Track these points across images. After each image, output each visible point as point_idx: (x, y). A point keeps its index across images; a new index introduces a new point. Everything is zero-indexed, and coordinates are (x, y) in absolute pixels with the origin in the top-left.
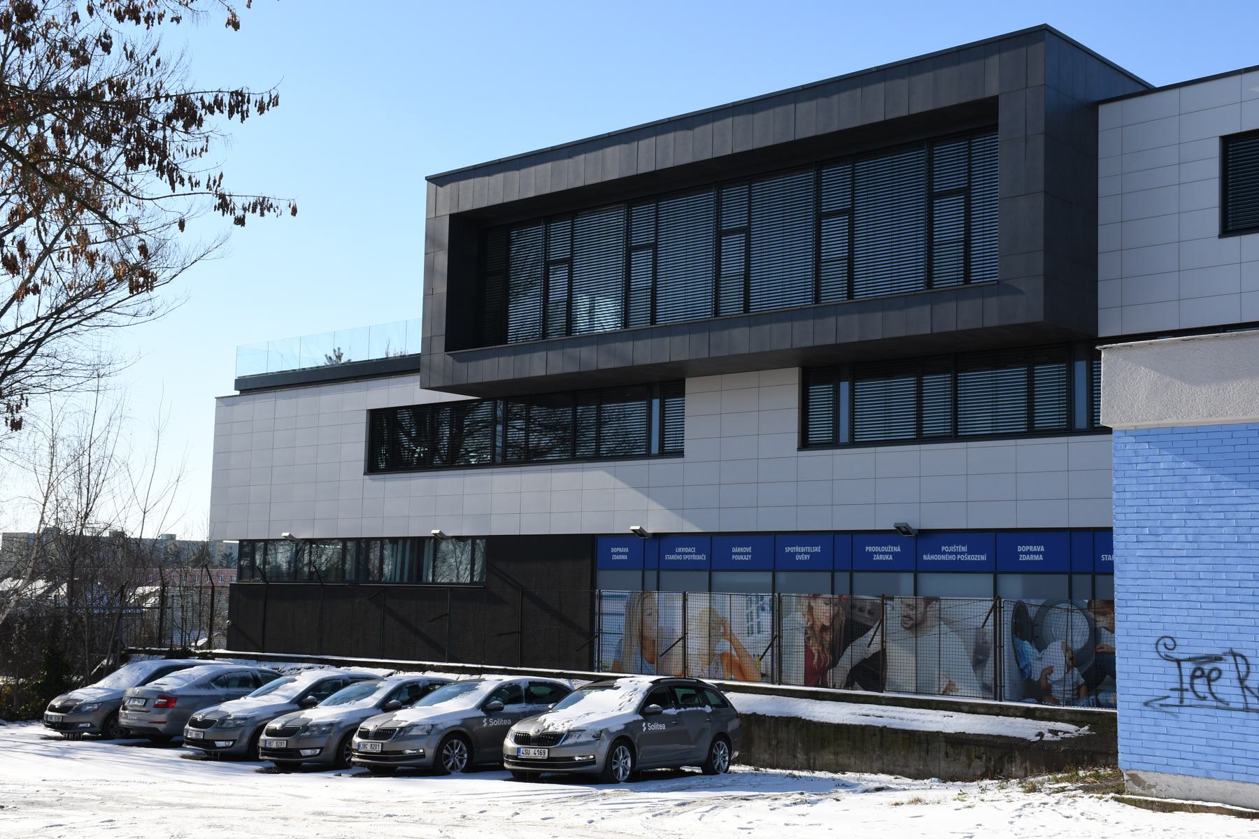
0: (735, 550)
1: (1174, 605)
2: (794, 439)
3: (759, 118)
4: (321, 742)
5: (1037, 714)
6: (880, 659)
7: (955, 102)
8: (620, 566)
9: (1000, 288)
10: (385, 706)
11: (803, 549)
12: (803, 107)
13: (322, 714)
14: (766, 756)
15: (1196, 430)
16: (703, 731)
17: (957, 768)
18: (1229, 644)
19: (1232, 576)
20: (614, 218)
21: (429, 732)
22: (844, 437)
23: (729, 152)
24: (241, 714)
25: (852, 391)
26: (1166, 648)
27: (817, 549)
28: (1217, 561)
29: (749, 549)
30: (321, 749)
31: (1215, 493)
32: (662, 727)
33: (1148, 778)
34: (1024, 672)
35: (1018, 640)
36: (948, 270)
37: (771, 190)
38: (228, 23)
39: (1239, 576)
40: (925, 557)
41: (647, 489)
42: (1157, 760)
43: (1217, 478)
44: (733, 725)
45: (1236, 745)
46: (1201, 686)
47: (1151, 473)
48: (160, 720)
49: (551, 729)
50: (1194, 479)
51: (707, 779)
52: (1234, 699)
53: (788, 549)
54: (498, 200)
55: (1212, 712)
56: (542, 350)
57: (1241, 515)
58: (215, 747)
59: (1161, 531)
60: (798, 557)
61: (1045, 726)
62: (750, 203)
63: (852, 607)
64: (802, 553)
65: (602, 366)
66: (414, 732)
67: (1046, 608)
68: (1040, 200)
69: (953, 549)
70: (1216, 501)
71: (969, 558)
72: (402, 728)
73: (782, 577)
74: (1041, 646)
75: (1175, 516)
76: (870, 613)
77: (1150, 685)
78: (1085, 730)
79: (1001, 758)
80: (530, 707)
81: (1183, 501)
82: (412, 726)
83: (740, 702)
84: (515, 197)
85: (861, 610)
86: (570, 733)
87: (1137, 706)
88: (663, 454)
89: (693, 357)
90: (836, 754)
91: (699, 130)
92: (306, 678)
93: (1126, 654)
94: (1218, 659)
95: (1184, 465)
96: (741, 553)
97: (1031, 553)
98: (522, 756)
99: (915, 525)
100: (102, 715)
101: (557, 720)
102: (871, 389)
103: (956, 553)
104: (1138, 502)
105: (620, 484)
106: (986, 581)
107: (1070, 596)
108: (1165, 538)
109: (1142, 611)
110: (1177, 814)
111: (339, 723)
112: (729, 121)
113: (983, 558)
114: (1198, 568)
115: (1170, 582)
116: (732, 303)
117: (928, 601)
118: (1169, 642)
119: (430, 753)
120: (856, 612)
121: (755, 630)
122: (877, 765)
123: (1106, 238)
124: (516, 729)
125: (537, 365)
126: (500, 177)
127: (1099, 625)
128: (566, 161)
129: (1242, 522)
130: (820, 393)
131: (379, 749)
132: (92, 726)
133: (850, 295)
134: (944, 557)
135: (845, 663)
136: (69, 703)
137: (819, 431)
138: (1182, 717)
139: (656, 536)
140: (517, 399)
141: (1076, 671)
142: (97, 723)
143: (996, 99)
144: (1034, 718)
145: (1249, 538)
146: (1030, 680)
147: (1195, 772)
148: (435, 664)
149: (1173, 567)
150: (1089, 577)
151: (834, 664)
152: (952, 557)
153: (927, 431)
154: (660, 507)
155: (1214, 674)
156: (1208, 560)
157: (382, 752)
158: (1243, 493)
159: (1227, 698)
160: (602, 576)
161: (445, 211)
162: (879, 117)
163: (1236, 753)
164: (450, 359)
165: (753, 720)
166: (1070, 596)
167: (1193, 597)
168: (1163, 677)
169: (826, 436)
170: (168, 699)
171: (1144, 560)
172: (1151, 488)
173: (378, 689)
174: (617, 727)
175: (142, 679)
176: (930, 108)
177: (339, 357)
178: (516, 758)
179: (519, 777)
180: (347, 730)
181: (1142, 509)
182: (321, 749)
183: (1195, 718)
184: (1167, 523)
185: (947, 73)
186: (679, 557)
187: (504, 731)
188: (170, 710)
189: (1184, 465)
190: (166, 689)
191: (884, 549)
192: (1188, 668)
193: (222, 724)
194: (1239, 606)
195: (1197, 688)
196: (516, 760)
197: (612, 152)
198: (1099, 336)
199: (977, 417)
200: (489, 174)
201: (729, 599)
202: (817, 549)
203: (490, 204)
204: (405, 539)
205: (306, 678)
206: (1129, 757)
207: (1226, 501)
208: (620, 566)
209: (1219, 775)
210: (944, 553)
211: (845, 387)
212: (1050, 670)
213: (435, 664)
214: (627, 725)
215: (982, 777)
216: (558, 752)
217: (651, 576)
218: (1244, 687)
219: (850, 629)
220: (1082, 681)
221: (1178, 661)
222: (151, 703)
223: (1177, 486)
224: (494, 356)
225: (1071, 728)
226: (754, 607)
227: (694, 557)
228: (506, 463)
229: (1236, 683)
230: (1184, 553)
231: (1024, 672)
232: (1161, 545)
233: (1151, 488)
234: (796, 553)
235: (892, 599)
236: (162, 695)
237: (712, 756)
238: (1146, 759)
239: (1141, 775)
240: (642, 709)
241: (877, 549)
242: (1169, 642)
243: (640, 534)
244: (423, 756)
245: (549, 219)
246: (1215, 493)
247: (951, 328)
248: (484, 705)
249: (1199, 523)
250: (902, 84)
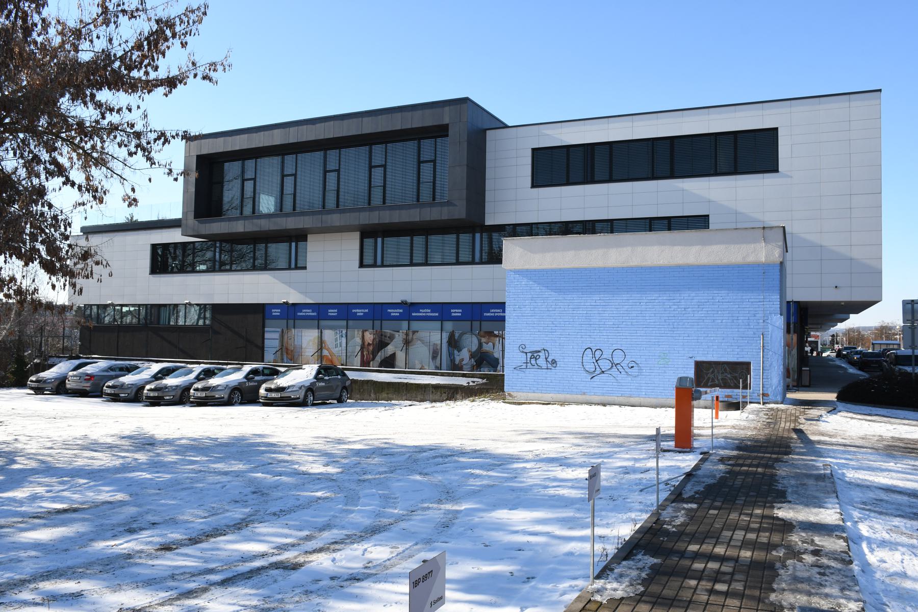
0: (329, 311)
1: (525, 333)
2: (357, 263)
3: (346, 122)
4: (173, 393)
5: (467, 375)
6: (393, 356)
7: (431, 124)
8: (276, 318)
9: (449, 203)
10: (198, 378)
11: (360, 311)
12: (365, 119)
13: (170, 381)
14: (358, 396)
15: (535, 271)
16: (338, 386)
17: (437, 397)
18: (543, 347)
19: (545, 323)
20: (276, 161)
21: (225, 388)
22: (379, 262)
23: (332, 137)
24: (130, 383)
25: (383, 243)
26: (522, 349)
27: (367, 311)
28: (541, 317)
29: (336, 311)
30: (173, 396)
31: (541, 293)
32: (324, 384)
33: (514, 394)
34: (453, 361)
35: (451, 349)
36: (426, 195)
37: (350, 154)
38: (164, 94)
39: (547, 323)
40: (413, 314)
41: (289, 284)
42: (517, 388)
43: (541, 288)
44: (348, 383)
45: (543, 381)
46: (533, 361)
47: (519, 286)
48: (87, 385)
49: (281, 386)
50: (534, 288)
51: (339, 405)
52: (544, 365)
53: (354, 311)
54: (221, 150)
55: (536, 370)
56: (242, 220)
57: (548, 301)
58: (120, 396)
59: (522, 307)
60: (358, 314)
61: (470, 380)
62: (340, 156)
63: (382, 335)
64: (360, 312)
65: (271, 229)
66: (219, 388)
67: (461, 335)
68: (465, 168)
69: (425, 311)
70: (540, 296)
71: (431, 314)
72: (214, 387)
73: (350, 322)
74: (459, 351)
75: (527, 301)
76: (389, 337)
77: (516, 361)
78: (485, 381)
79: (453, 393)
80: (264, 378)
81: (530, 296)
82: (218, 386)
83: (351, 375)
84: (229, 149)
85: (385, 336)
86: (289, 387)
87: (511, 369)
88: (297, 268)
89: (314, 226)
90: (387, 394)
91: (318, 125)
92: (156, 367)
93: (509, 351)
94: (539, 352)
95: (531, 283)
96: (333, 312)
97: (456, 313)
98: (269, 396)
99: (409, 301)
100: (56, 383)
101: (281, 382)
102: (391, 241)
103: (426, 313)
104: (515, 296)
105: (277, 281)
106: (438, 324)
107: (471, 330)
108: (524, 309)
109: (515, 335)
110: (523, 405)
111: (180, 385)
112: (332, 123)
113: (437, 314)
114: (534, 320)
115: (525, 325)
116: (331, 203)
117: (414, 332)
118: (523, 346)
119: (226, 396)
120: (383, 337)
121: (339, 346)
122: (404, 397)
123: (489, 185)
124: (264, 386)
125: (239, 227)
126: (222, 139)
127: (482, 341)
128: (255, 134)
129: (549, 304)
130: (369, 242)
131: (204, 395)
132: (52, 389)
133: (384, 203)
134: (421, 314)
135: (379, 358)
136: (40, 379)
137: (368, 260)
138: (526, 372)
139: (293, 304)
140: (226, 241)
141: (473, 360)
142: (54, 387)
143: (447, 125)
144: (466, 377)
145: (551, 309)
146: (454, 364)
147: (530, 391)
148: (205, 361)
149: (526, 320)
150: (479, 322)
151: (373, 359)
152: (424, 314)
153: (414, 261)
154: (295, 291)
155: (538, 357)
156: (537, 317)
157: (206, 397)
158: (550, 293)
159: (541, 365)
160: (267, 322)
161: (194, 153)
162: (399, 128)
163: (543, 384)
164: (196, 222)
165: (354, 382)
166: (471, 330)
167: (532, 330)
168: (521, 358)
169: (371, 262)
170: (91, 377)
171: (516, 317)
172: (519, 291)
173: (194, 371)
174: (308, 384)
175: (72, 368)
176: (420, 126)
177: (132, 218)
178: (266, 397)
179: (265, 405)
180: (187, 389)
181: (516, 299)
182: (173, 396)
183: (531, 372)
184: (524, 304)
185: (428, 112)
186: (304, 314)
187: (259, 387)
188: (91, 382)
189: (531, 283)
190: (89, 372)
191: (395, 311)
192: (529, 355)
193: (122, 386)
194: (547, 333)
195: (532, 362)
196: (266, 398)
197: (276, 132)
198: (487, 224)
199: (436, 257)
200: (216, 138)
201: (66, 332)
202: (367, 311)
203: (217, 151)
204: (170, 305)
205: (156, 367)
206: (508, 387)
207: (544, 296)
208: (276, 318)
209: (537, 391)
210: (421, 312)
211: (379, 240)
212: (463, 360)
213: (205, 361)
214: (311, 383)
215: (447, 400)
216: (284, 394)
217: (291, 322)
218: (547, 361)
219: (381, 344)
220: (475, 363)
221: (526, 353)
222: (82, 379)
223: (528, 291)
224: (219, 222)
225: (480, 380)
226: (338, 336)
227: (311, 314)
228: (221, 271)
229: (545, 360)
230: (530, 315)
231: (453, 361)
232: (522, 312)
233: (519, 291)
234: (357, 312)
235: (398, 332)
236: (88, 375)
237: (341, 396)
238: (514, 388)
239: (512, 393)
240: (316, 377)
241: (393, 311)
242: (523, 346)
243: (286, 303)
244: (223, 398)
245: (244, 159)
246: (541, 293)
247: (428, 219)
248: (246, 377)
249: (535, 304)
250: (409, 114)
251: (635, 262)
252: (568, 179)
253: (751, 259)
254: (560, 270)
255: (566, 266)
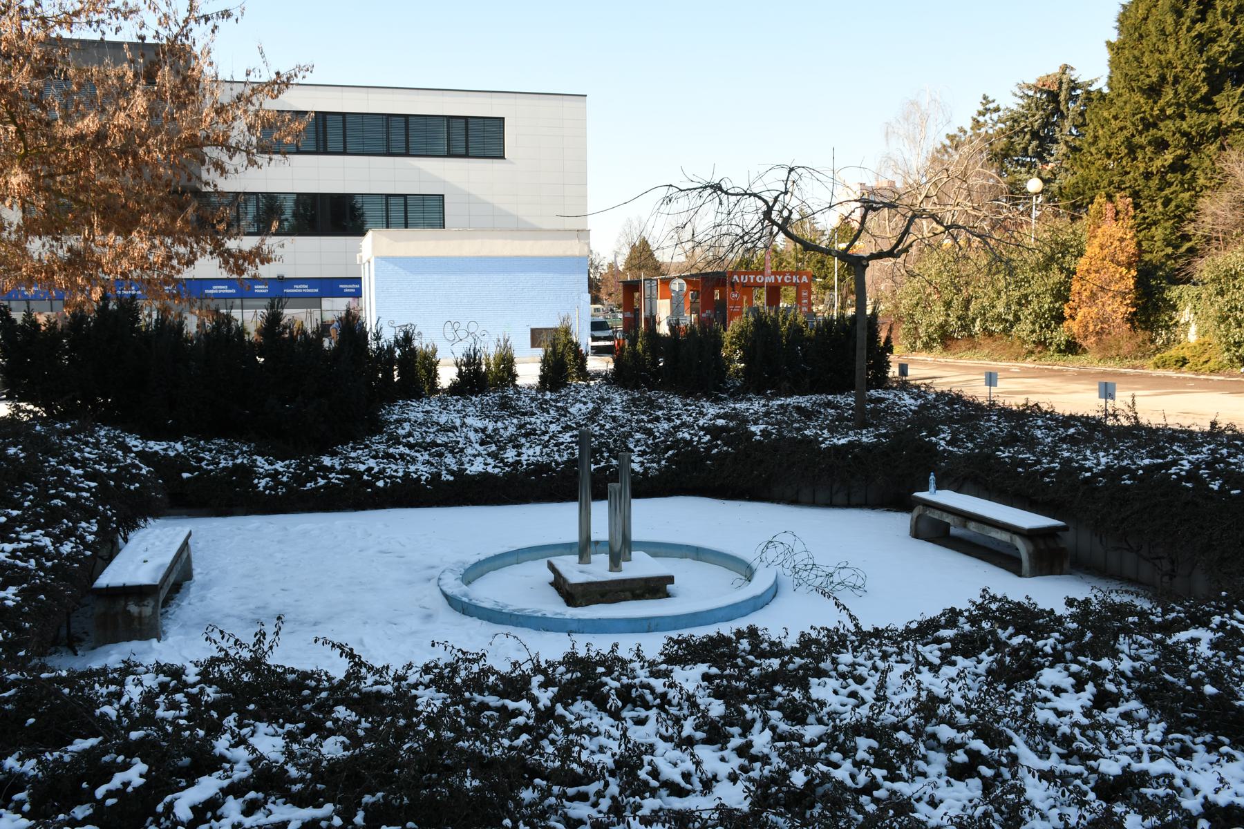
15: (400, 258)
53: (341, 286)
69: (300, 286)
113: (317, 290)
227: (227, 291)
251: (456, 253)
252: (388, 149)
253: (569, 253)
254: (422, 257)
255: (428, 255)
